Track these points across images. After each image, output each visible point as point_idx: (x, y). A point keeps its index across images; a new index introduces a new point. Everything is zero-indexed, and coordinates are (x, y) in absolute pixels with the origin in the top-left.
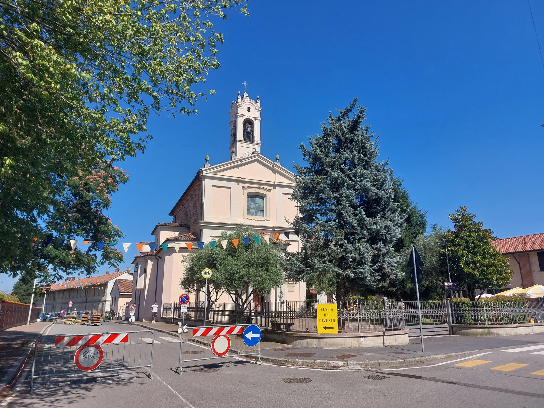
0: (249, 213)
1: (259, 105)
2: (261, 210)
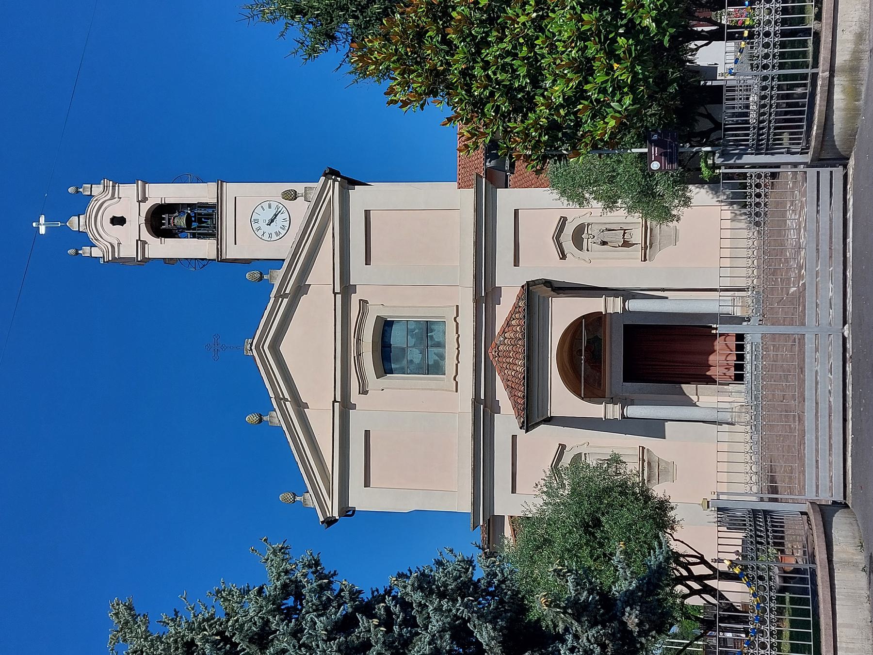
0: (436, 368)
1: (97, 189)
2: (427, 332)
